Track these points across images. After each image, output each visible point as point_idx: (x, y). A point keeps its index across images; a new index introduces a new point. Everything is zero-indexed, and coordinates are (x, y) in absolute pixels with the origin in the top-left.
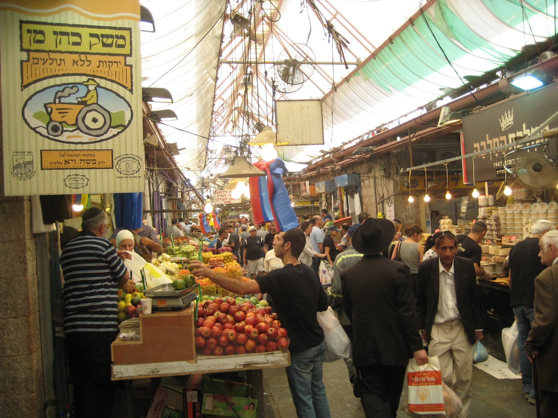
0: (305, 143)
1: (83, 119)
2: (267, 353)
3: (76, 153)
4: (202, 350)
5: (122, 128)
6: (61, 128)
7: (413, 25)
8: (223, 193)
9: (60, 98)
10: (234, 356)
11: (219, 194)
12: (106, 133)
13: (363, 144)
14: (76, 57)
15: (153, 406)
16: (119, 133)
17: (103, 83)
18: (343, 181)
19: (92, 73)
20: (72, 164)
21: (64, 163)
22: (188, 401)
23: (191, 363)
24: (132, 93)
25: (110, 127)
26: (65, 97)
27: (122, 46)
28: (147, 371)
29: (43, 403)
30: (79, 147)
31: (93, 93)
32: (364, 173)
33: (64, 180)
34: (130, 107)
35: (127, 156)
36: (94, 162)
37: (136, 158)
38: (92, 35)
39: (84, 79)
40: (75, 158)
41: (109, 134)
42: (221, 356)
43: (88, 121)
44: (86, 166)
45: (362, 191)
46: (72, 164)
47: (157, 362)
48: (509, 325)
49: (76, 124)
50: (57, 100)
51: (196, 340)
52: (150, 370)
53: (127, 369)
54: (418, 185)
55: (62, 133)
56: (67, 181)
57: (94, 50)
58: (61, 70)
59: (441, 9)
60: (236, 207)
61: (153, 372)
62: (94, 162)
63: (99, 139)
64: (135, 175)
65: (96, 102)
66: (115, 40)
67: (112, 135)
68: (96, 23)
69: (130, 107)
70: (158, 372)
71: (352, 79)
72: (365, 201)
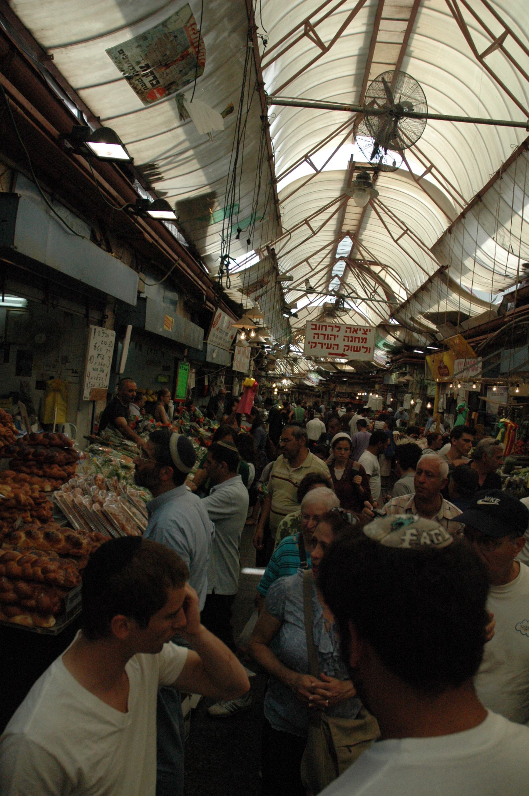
8: (329, 329)
11: (320, 332)
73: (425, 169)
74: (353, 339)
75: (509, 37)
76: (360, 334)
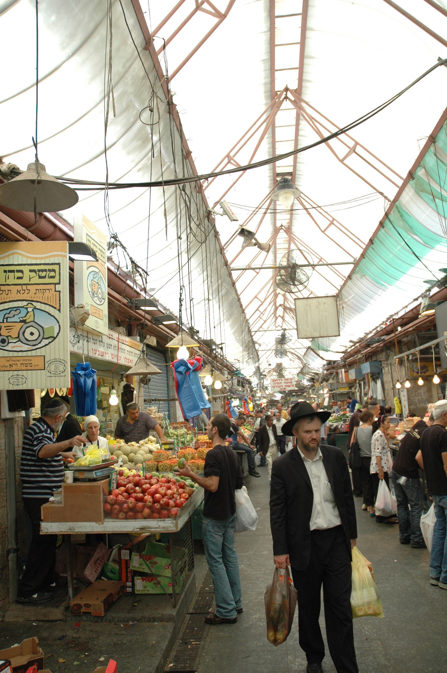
0: (322, 335)
1: (24, 333)
2: (160, 519)
3: (17, 359)
4: (109, 514)
5: (52, 339)
6: (7, 341)
7: (383, 227)
9: (7, 318)
10: (126, 520)
12: (40, 343)
13: (380, 334)
14: (19, 288)
15: (92, 560)
16: (50, 343)
17: (38, 305)
18: (366, 368)
19: (30, 299)
20: (14, 367)
21: (9, 366)
22: (122, 558)
23: (99, 524)
24: (60, 312)
25: (43, 338)
26: (10, 318)
27: (53, 277)
28: (66, 528)
29: (5, 550)
30: (20, 354)
31: (31, 314)
32: (384, 360)
33: (9, 379)
34: (58, 323)
35: (55, 360)
36: (31, 365)
37: (62, 361)
38: (31, 271)
39: (25, 303)
40: (17, 362)
41: (43, 344)
42: (123, 520)
43: (27, 335)
44: (25, 368)
45: (384, 377)
46: (14, 367)
47: (74, 522)
48: (426, 510)
49: (18, 337)
50: (5, 320)
51: (104, 506)
52: (68, 528)
53: (51, 526)
54: (428, 370)
55: (8, 344)
56: (10, 379)
57: (32, 282)
58: (8, 298)
59: (399, 212)
60: (296, 393)
61: (70, 529)
62: (31, 365)
63: (35, 347)
64: (62, 374)
65: (33, 320)
66: (48, 272)
67: (44, 345)
68: (34, 262)
69: (58, 323)
70: (74, 529)
71: (353, 276)
72: (386, 386)
73: (329, 222)
74: (287, 383)
75: (358, 146)
76: (289, 381)
